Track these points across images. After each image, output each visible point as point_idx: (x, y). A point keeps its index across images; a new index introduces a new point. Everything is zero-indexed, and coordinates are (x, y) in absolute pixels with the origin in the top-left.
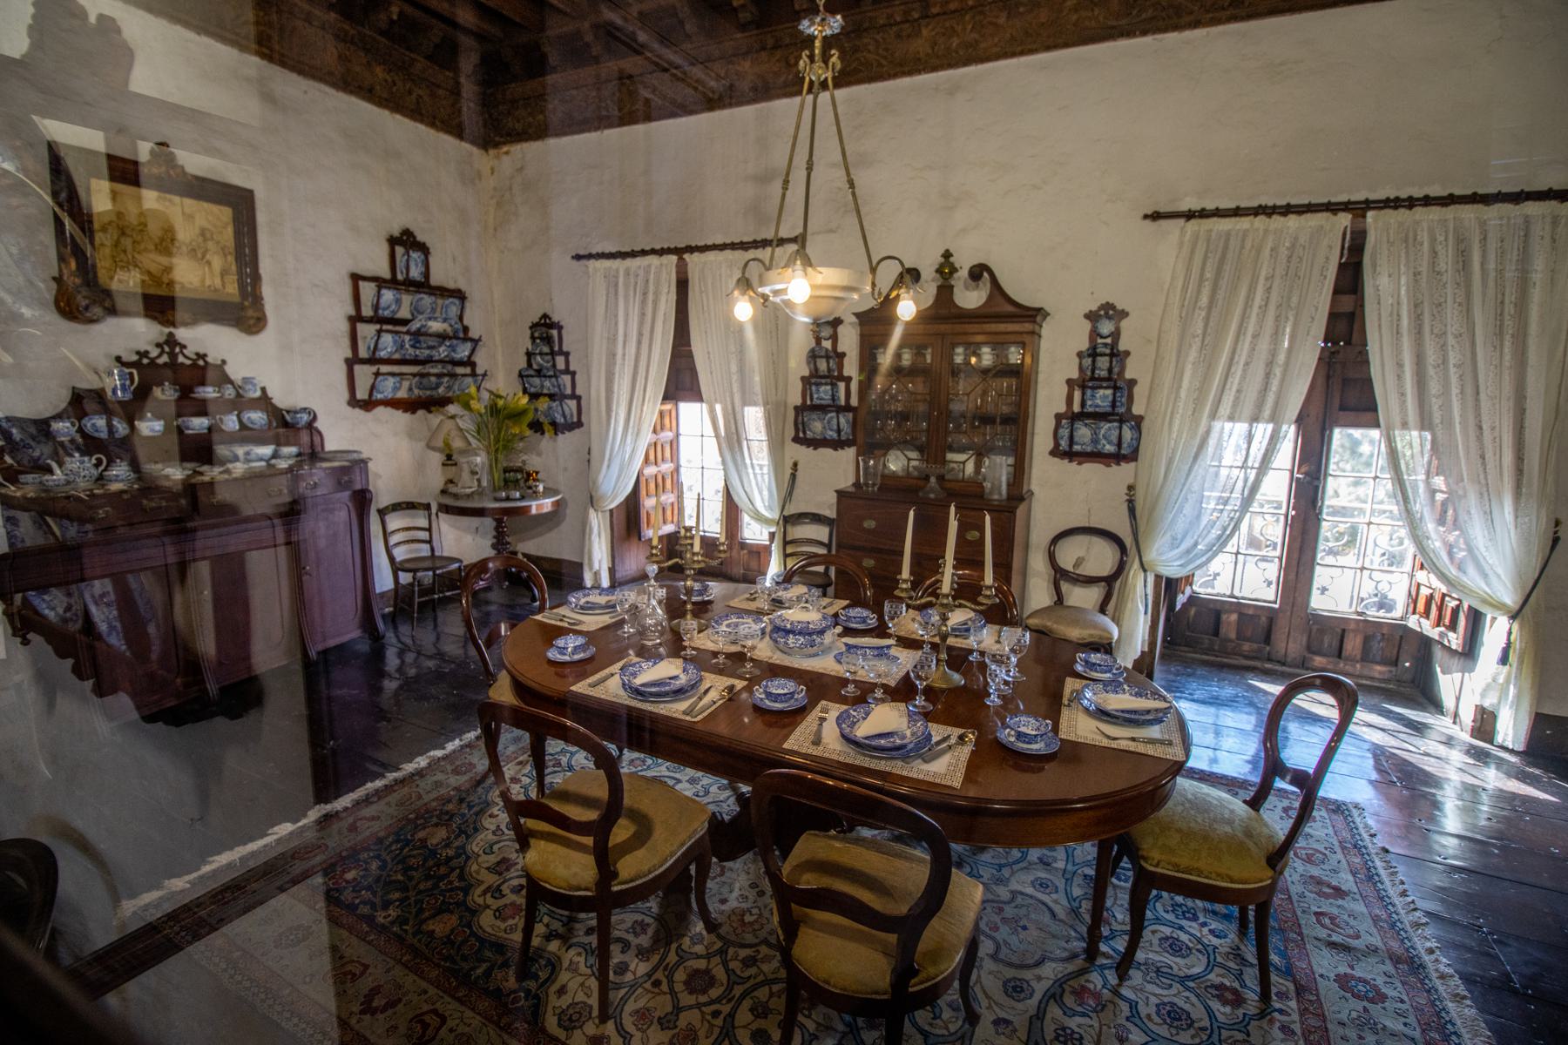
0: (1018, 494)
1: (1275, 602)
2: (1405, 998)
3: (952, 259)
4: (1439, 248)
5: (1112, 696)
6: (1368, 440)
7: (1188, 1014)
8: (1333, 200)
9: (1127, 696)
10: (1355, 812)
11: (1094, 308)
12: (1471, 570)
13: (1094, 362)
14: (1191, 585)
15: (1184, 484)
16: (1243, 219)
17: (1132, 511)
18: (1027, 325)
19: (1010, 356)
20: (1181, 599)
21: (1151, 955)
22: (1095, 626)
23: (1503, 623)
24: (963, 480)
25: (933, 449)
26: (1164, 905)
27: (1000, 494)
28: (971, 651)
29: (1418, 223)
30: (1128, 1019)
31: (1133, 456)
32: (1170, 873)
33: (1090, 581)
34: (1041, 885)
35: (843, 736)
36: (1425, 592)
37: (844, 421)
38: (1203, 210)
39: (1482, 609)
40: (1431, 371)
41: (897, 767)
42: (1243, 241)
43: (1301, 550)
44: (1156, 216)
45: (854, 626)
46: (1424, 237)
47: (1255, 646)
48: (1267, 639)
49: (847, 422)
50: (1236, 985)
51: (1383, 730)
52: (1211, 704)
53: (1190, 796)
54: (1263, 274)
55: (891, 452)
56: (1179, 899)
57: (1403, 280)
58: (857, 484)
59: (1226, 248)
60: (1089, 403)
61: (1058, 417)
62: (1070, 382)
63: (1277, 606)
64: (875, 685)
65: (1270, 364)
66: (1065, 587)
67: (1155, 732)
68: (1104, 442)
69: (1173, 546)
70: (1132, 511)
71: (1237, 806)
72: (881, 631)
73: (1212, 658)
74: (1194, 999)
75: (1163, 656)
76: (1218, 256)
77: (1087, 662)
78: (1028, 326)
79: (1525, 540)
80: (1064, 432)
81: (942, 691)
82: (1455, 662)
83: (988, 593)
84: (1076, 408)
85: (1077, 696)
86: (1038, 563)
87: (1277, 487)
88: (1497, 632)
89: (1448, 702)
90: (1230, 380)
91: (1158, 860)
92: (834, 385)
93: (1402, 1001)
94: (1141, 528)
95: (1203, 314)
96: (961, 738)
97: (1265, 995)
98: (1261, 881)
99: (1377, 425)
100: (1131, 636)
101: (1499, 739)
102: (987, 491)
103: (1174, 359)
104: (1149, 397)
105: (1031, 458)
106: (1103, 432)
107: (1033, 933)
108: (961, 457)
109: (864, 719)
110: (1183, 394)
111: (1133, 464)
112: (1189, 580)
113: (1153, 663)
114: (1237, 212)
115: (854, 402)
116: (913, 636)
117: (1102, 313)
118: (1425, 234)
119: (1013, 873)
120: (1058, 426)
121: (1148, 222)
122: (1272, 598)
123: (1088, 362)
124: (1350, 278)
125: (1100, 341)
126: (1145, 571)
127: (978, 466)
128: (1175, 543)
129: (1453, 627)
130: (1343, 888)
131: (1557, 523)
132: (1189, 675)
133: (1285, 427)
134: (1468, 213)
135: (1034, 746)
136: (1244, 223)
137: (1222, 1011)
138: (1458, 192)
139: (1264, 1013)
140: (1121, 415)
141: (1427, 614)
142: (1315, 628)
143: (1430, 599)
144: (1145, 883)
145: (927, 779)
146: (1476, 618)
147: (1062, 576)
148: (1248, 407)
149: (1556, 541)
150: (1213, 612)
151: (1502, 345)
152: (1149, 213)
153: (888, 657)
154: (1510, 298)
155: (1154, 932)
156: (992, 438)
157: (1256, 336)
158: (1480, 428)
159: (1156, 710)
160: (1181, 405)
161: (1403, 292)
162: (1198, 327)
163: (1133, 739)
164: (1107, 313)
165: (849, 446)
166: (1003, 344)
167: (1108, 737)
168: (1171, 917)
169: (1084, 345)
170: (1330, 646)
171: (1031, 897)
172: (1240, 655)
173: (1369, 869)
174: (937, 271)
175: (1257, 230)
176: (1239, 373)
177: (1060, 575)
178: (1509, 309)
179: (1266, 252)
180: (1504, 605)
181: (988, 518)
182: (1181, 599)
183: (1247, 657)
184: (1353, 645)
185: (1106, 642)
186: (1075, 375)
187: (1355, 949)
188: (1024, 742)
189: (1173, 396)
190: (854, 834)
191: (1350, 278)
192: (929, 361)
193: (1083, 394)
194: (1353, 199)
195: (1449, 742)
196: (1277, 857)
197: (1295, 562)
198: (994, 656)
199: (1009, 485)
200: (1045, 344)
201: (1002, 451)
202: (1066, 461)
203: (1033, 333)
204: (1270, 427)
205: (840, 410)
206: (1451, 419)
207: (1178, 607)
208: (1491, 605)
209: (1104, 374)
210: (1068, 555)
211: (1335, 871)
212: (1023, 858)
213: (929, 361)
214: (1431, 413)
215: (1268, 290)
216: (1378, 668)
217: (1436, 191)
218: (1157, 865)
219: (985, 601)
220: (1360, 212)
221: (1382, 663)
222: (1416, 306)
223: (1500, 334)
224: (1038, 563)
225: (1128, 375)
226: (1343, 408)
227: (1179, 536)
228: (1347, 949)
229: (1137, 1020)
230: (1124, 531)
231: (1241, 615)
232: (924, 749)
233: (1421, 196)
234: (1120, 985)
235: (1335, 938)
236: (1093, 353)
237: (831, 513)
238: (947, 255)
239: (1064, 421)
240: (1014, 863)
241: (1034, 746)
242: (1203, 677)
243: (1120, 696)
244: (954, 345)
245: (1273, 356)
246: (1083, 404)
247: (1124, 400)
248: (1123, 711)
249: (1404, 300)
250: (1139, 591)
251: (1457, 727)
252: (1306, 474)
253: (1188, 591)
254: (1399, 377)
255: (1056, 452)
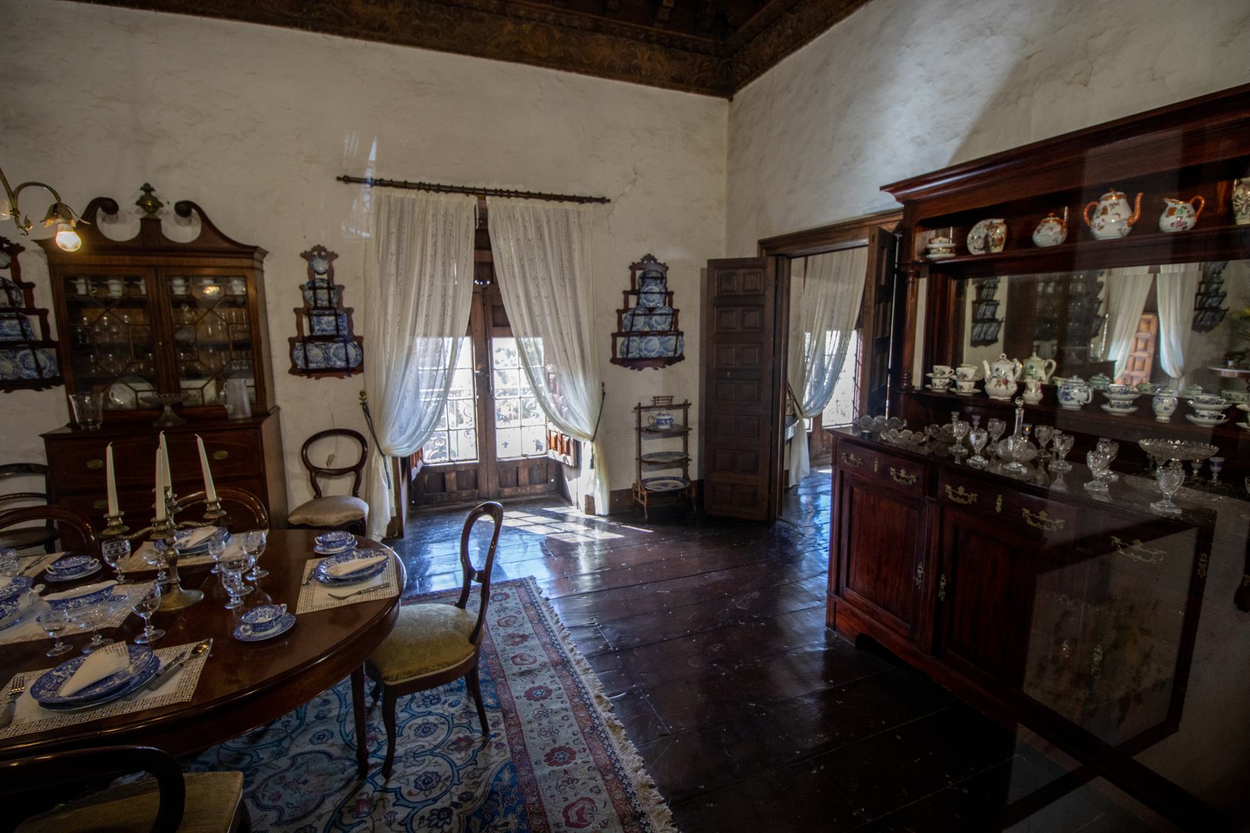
0: (263, 408)
1: (477, 459)
2: (561, 686)
3: (153, 194)
4: (527, 224)
5: (343, 564)
6: (509, 344)
7: (436, 773)
8: (466, 186)
9: (356, 560)
10: (530, 582)
11: (308, 249)
12: (571, 419)
13: (315, 294)
14: (422, 459)
15: (401, 386)
16: (411, 191)
17: (366, 411)
18: (245, 261)
19: (235, 288)
20: (415, 471)
21: (409, 746)
22: (349, 508)
23: (589, 443)
24: (204, 405)
25: (166, 380)
26: (417, 703)
27: (244, 413)
28: (213, 565)
29: (514, 207)
30: (394, 805)
31: (359, 369)
32: (407, 680)
33: (341, 473)
34: (319, 738)
35: (44, 704)
36: (553, 435)
37: (45, 358)
38: (381, 180)
39: (579, 439)
40: (534, 301)
41: (120, 708)
42: (413, 206)
43: (486, 421)
44: (603, 200)
45: (70, 577)
46: (518, 216)
47: (469, 491)
48: (476, 486)
49: (50, 359)
50: (468, 734)
51: (543, 525)
52: (444, 541)
53: (417, 616)
54: (430, 232)
55: (115, 386)
56: (427, 693)
57: (512, 244)
58: (72, 424)
59: (402, 211)
60: (317, 328)
61: (292, 341)
62: (296, 310)
63: (478, 461)
64: (91, 634)
65: (444, 296)
66: (321, 482)
67: (378, 580)
68: (334, 359)
69: (402, 433)
70: (366, 411)
71: (451, 610)
72: (106, 573)
73: (445, 508)
74: (440, 760)
75: (411, 516)
76: (398, 215)
77: (323, 542)
78: (247, 262)
79: (591, 397)
80: (299, 354)
81: (179, 612)
82: (573, 473)
83: (213, 508)
84: (307, 333)
85: (315, 573)
86: (294, 467)
87: (463, 380)
88: (588, 449)
89: (574, 499)
90: (420, 308)
91: (396, 674)
92: (22, 320)
93: (560, 689)
94: (376, 424)
95: (394, 258)
96: (195, 652)
97: (485, 730)
98: (468, 655)
99: (511, 335)
100: (381, 507)
101: (597, 512)
102: (230, 412)
103: (378, 291)
104: (365, 321)
105: (272, 377)
106: (332, 351)
107: (314, 781)
108: (199, 383)
109: (72, 674)
110: (389, 318)
111: (360, 375)
112: (419, 454)
113: (401, 524)
114: (405, 185)
115: (54, 336)
116: (148, 568)
117: (316, 253)
118: (519, 215)
119: (292, 740)
120: (292, 348)
121: (341, 183)
122: (474, 457)
123: (310, 294)
124: (483, 241)
125: (317, 276)
126: (383, 456)
127: (219, 389)
128: (402, 431)
129: (568, 453)
130: (526, 634)
131: (603, 385)
132: (429, 525)
133: (460, 339)
134: (539, 204)
135: (271, 631)
136: (412, 194)
137: (458, 758)
138: (410, 180)
139: (485, 743)
140: (344, 335)
141: (556, 448)
142: (502, 470)
143: (556, 438)
144: (389, 695)
145: (154, 706)
146: (577, 445)
147: (317, 473)
148: (435, 328)
149: (604, 394)
150: (438, 476)
151: (565, 285)
152: (341, 176)
153: (113, 599)
154: (565, 257)
155: (410, 728)
156: (228, 363)
157: (432, 276)
158: (562, 334)
159: (378, 564)
160: (390, 326)
161: (513, 251)
162: (392, 269)
163: (360, 593)
164: (319, 254)
165: (58, 385)
166: (228, 277)
167: (339, 598)
168: (422, 709)
169: (305, 280)
170: (512, 480)
171: (310, 752)
172: (461, 500)
173: (539, 615)
174: (138, 203)
175: (421, 200)
176: (425, 302)
177: (315, 473)
178: (566, 264)
179: (429, 217)
180: (588, 435)
181: (200, 441)
182: (415, 471)
183: (466, 501)
184: (524, 476)
185: (359, 518)
186: (301, 305)
187: (534, 670)
188: (261, 631)
189: (382, 320)
190: (113, 787)
191: (483, 241)
192: (144, 292)
193: (310, 321)
194: (477, 187)
195: (577, 521)
196: (475, 635)
197: (484, 430)
198: (231, 563)
199: (251, 404)
200: (268, 279)
201: (241, 374)
202: (305, 377)
203: (253, 268)
204: (451, 339)
205: (34, 346)
206: (547, 329)
207: (414, 477)
208: (583, 436)
209: (325, 303)
210: (320, 455)
211: (522, 625)
212: (302, 719)
213: (144, 292)
214: (537, 326)
215: (435, 244)
216: (539, 487)
217: (521, 189)
218: (397, 679)
219: (211, 517)
220: (482, 196)
221: (539, 484)
222: (520, 260)
223: (563, 278)
224: (294, 467)
225: (346, 304)
226: (495, 325)
227: (404, 425)
228: (529, 672)
229: (402, 802)
230: (362, 428)
231: (458, 473)
232: (152, 677)
233: (514, 190)
234: (386, 783)
235: (524, 668)
236: (313, 286)
237: (42, 460)
238: (148, 189)
239: (297, 344)
240: (293, 732)
241: (271, 631)
242: (439, 523)
243: (351, 562)
244: (171, 278)
245: (445, 290)
246: (311, 329)
247: (345, 324)
248: (352, 573)
249: (514, 256)
250: (382, 472)
251: (579, 510)
252: (481, 370)
253: (420, 464)
254: (518, 304)
255: (294, 371)
